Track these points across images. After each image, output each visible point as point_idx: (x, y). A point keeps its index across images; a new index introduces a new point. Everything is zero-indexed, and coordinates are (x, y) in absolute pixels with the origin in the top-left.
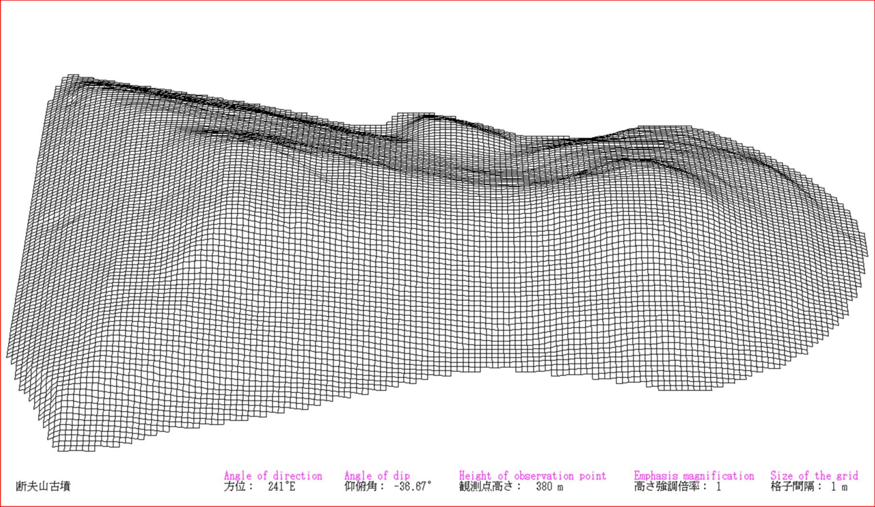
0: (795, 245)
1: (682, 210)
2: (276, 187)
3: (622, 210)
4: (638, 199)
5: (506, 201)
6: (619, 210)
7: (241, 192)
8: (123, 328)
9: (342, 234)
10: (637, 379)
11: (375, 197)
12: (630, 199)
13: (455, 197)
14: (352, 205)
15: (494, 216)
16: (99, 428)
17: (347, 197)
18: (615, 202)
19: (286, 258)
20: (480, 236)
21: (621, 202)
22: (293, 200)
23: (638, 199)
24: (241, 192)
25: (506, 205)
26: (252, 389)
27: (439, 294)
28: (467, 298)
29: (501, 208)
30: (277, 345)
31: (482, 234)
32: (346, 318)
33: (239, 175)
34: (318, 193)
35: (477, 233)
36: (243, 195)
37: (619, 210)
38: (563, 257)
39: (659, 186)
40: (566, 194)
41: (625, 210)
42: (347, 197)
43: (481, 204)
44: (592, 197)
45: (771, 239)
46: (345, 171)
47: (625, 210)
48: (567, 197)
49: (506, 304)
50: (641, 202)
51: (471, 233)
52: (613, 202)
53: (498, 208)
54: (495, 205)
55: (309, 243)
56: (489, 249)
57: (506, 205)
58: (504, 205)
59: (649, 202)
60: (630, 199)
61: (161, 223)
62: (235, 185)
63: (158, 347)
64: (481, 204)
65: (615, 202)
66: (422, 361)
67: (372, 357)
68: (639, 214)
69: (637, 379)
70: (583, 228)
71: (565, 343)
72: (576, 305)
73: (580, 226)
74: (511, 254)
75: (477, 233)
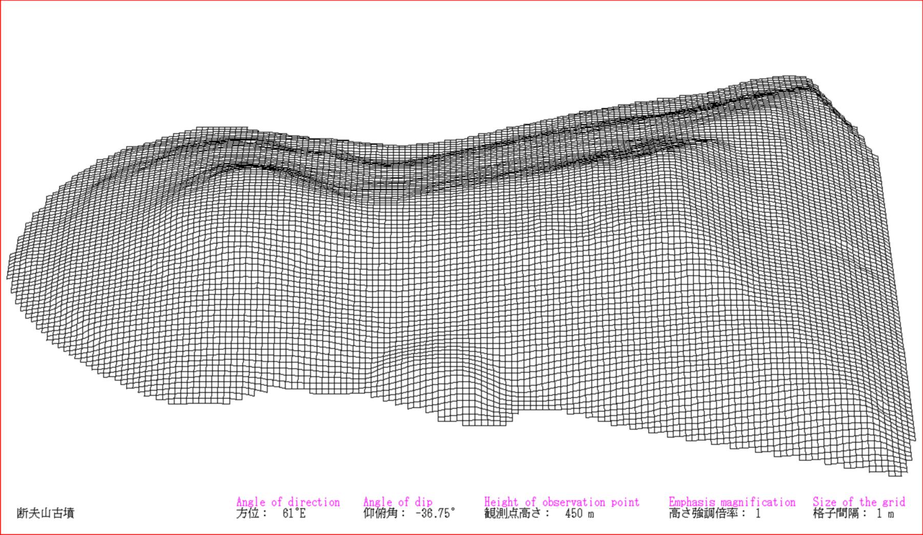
0: (830, 328)
1: (694, 231)
2: (304, 200)
3: (565, 213)
4: (676, 191)
5: (265, 194)
7: (382, 210)
9: (307, 252)
11: (324, 206)
12: (674, 198)
13: (265, 194)
14: (372, 217)
15: (677, 228)
17: (304, 204)
18: (668, 217)
19: (219, 275)
20: (349, 263)
21: (675, 221)
22: (286, 214)
23: (676, 191)
24: (382, 210)
25: (443, 216)
26: (266, 330)
27: (299, 313)
28: (368, 305)
29: (390, 214)
31: (352, 261)
32: (324, 306)
34: (330, 207)
35: (346, 260)
36: (312, 205)
37: (568, 212)
39: (779, 161)
40: (598, 197)
41: (562, 213)
42: (304, 204)
43: (244, 208)
44: (589, 187)
45: (807, 326)
46: (263, 187)
48: (645, 215)
49: (265, 341)
50: (670, 195)
51: (340, 260)
52: (671, 217)
53: (387, 214)
54: (503, 219)
55: (231, 262)
56: (370, 277)
57: (443, 216)
58: (441, 216)
59: (779, 330)
60: (674, 198)
61: (111, 243)
62: (244, 194)
63: (781, 372)
64: (244, 208)
65: (668, 217)
66: (311, 334)
67: (550, 264)
68: (557, 232)
70: (541, 245)
71: (484, 305)
72: (399, 325)
74: (382, 283)
75: (346, 260)
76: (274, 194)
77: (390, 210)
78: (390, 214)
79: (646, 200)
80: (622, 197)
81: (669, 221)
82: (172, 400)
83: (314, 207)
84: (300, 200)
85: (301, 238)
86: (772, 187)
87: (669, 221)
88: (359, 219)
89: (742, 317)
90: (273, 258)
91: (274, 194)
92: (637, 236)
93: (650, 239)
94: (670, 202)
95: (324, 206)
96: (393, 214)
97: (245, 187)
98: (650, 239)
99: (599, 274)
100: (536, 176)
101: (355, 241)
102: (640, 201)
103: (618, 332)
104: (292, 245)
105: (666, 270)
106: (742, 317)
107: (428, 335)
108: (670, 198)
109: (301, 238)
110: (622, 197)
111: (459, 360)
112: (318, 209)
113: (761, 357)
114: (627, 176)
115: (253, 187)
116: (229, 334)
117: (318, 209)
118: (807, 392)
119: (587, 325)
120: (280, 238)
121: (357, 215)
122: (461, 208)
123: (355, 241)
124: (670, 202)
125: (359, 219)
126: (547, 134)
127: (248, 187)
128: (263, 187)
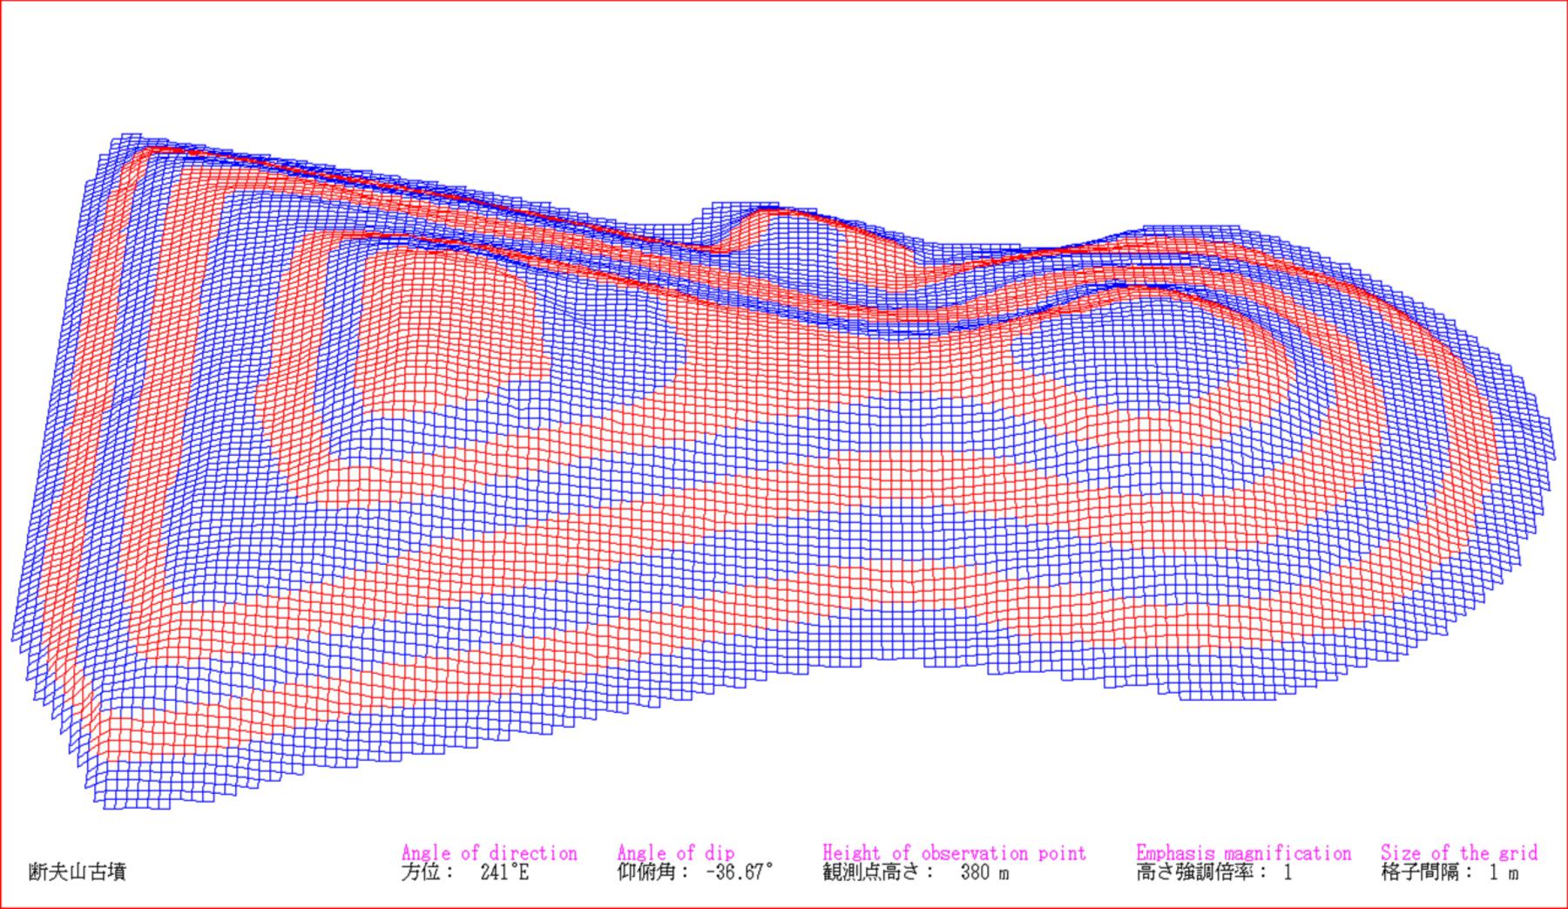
2: (494, 336)
3: (1114, 376)
6: (1109, 377)
8: (220, 588)
10: (1142, 680)
11: (673, 353)
12: (1128, 356)
16: (1118, 573)
17: (621, 354)
18: (1103, 362)
29: (897, 373)
30: (497, 618)
33: (428, 315)
36: (611, 359)
37: (1109, 377)
38: (1094, 503)
41: (1120, 376)
44: (1061, 354)
46: (619, 307)
47: (1120, 376)
52: (1098, 363)
60: (1128, 356)
63: (528, 673)
65: (1103, 362)
69: (1142, 680)
73: (1040, 405)
76: (423, 315)
77: (897, 367)
78: (897, 373)
79: (1061, 360)
80: (1025, 353)
81: (1109, 362)
82: (1269, 694)
83: (614, 363)
84: (488, 334)
85: (475, 502)
86: (659, 334)
87: (1119, 356)
88: (596, 396)
89: (1125, 390)
90: (593, 609)
91: (423, 315)
92: (1013, 388)
93: (1065, 377)
94: (1163, 356)
95: (673, 353)
96: (903, 373)
97: (603, 302)
98: (1065, 377)
99: (772, 603)
100: (944, 336)
101: (622, 481)
102: (1036, 357)
103: (166, 777)
104: (824, 443)
105: (709, 626)
106: (1125, 390)
107: (968, 368)
108: (1122, 356)
109: (475, 502)
110: (1025, 353)
111: (1141, 383)
112: (621, 366)
113: (1127, 538)
114: (624, 307)
115: (425, 293)
116: (1117, 564)
117: (621, 366)
118: (1182, 599)
119: (1084, 514)
120: (490, 509)
121: (626, 386)
122: (857, 366)
123: (622, 481)
124: (1163, 356)
125: (596, 396)
126: (1000, 320)
127: (599, 302)
128: (619, 307)
